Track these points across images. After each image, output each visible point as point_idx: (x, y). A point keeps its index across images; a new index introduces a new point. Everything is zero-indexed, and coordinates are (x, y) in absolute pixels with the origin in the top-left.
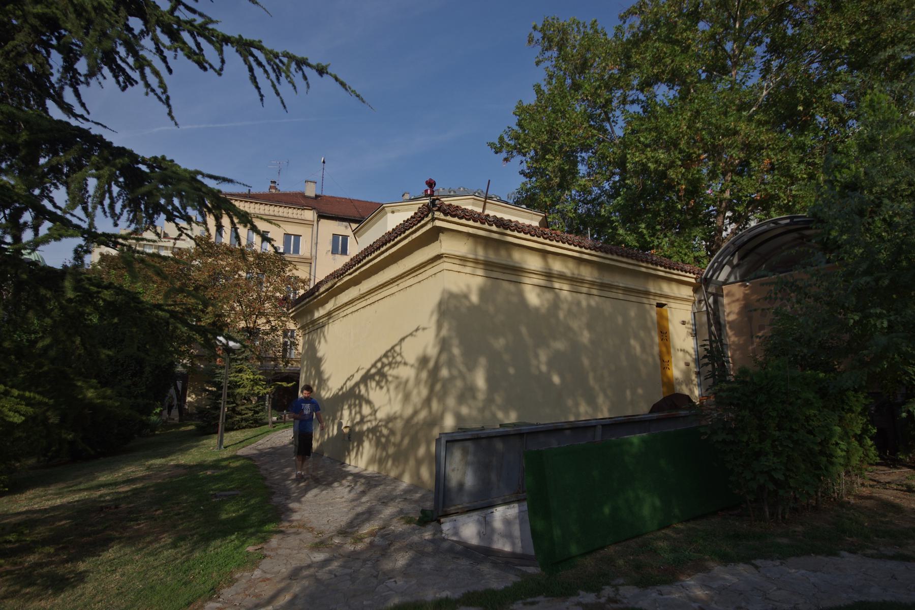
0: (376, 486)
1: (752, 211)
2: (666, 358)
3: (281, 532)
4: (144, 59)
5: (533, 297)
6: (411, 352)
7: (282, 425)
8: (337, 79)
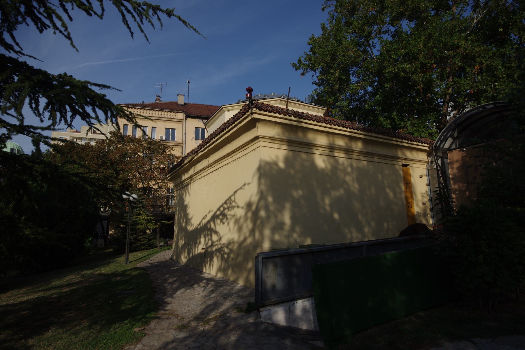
0: (221, 286)
1: (467, 101)
2: (410, 200)
3: (158, 318)
4: (50, 9)
5: (320, 161)
6: (242, 199)
7: (166, 248)
8: (180, 19)
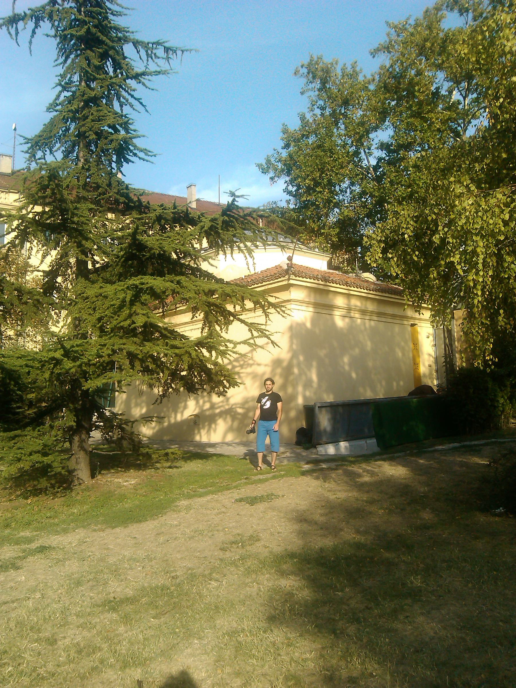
5: (340, 322)
